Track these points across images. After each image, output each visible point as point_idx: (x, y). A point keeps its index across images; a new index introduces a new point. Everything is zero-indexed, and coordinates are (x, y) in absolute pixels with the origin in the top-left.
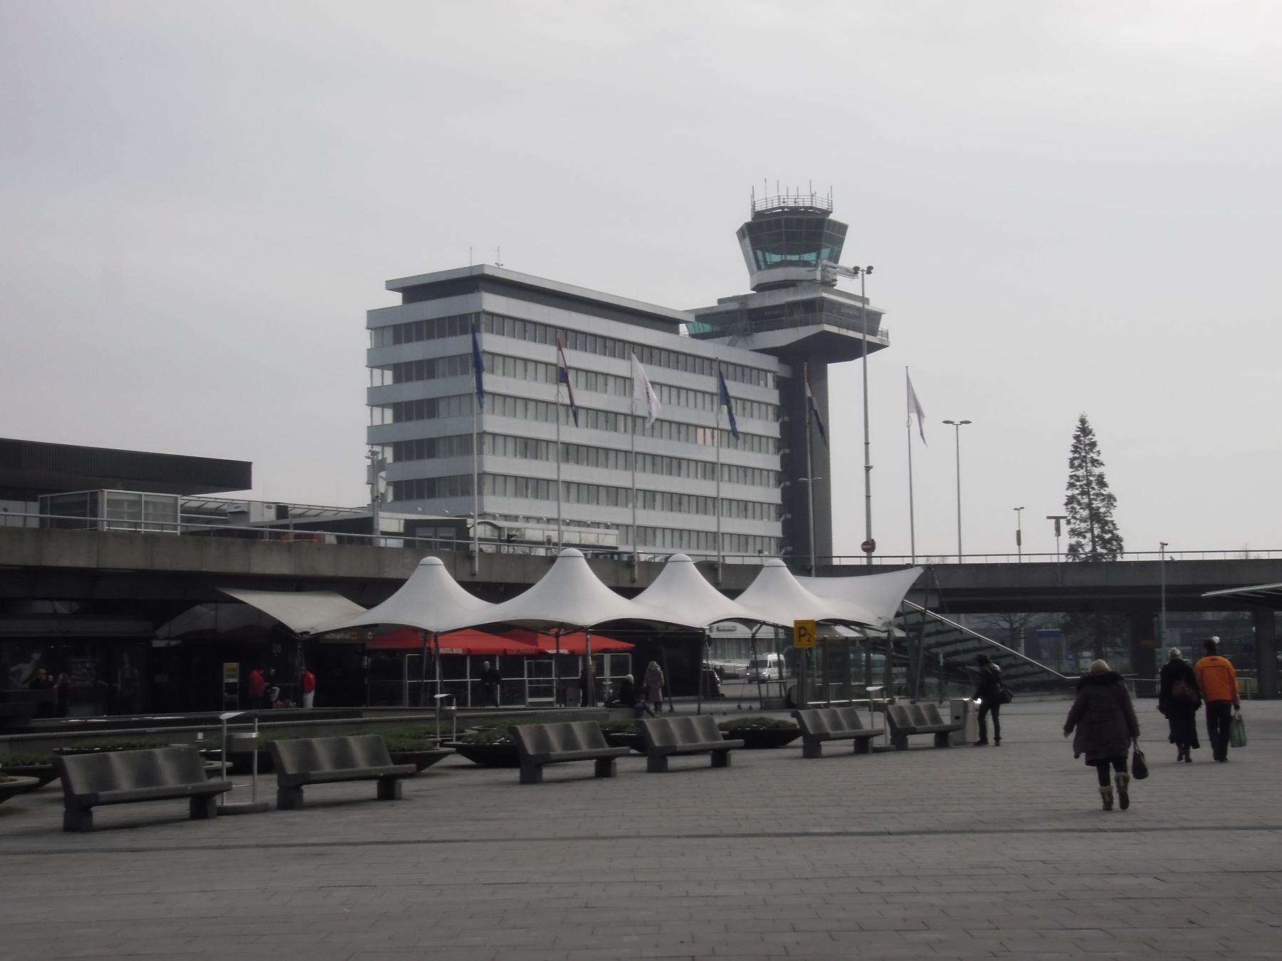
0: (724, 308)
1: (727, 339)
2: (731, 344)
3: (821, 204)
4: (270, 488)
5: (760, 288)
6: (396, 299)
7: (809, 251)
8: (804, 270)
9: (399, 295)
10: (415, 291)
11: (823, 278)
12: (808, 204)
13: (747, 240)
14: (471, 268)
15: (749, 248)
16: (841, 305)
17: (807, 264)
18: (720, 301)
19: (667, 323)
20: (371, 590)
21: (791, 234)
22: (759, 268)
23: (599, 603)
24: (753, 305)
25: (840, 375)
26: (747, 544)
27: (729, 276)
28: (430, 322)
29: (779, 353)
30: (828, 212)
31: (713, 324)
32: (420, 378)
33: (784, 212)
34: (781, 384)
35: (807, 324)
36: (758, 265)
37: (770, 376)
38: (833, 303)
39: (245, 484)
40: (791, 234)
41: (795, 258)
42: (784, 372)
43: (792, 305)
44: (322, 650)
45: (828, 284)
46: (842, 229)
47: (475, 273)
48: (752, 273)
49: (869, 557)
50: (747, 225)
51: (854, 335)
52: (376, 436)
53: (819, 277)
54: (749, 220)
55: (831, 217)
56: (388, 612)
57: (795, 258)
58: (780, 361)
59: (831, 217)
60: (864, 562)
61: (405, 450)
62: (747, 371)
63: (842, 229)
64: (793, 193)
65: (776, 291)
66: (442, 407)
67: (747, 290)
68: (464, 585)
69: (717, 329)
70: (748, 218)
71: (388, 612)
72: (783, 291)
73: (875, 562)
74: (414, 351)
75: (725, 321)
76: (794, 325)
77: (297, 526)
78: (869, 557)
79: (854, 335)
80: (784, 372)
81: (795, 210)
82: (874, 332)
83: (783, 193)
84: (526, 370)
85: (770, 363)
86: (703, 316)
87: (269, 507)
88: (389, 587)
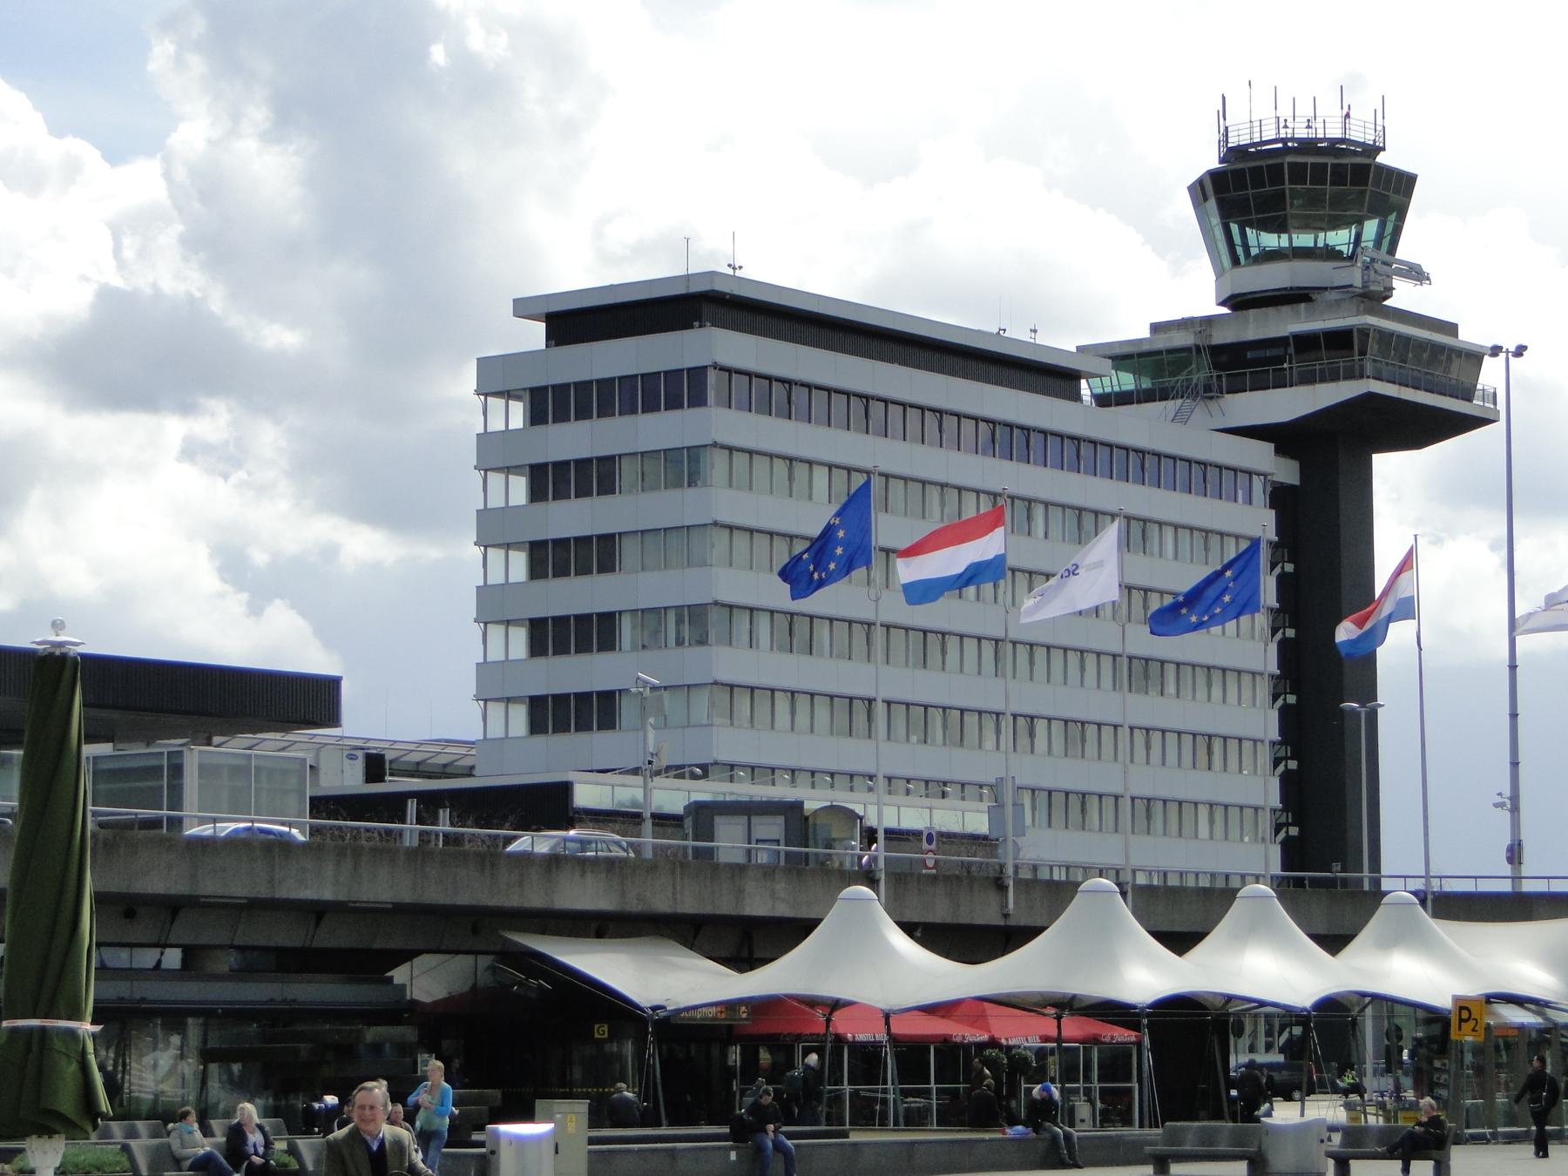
0: (1162, 343)
1: (1171, 405)
2: (1178, 418)
3: (1360, 133)
4: (365, 718)
5: (1238, 302)
6: (534, 335)
7: (1335, 224)
8: (1328, 266)
9: (540, 328)
10: (572, 322)
11: (1365, 284)
12: (1335, 132)
13: (1212, 204)
14: (688, 278)
15: (1215, 220)
16: (1406, 340)
17: (1331, 254)
18: (1156, 328)
19: (1054, 377)
20: (747, 942)
21: (1297, 194)
22: (1236, 261)
23: (1146, 975)
24: (1221, 337)
25: (1396, 476)
26: (1149, 816)
27: (1170, 280)
28: (605, 384)
29: (1281, 437)
30: (1377, 149)
31: (1137, 372)
32: (583, 492)
33: (1286, 150)
34: (1280, 497)
35: (1335, 378)
36: (1234, 255)
37: (1257, 483)
38: (1385, 337)
39: (331, 717)
40: (1297, 194)
41: (1304, 240)
42: (1287, 472)
43: (1306, 343)
44: (685, 1040)
45: (1374, 298)
46: (1404, 183)
47: (695, 288)
48: (1220, 273)
49: (1516, 878)
50: (1214, 175)
51: (1427, 391)
52: (492, 606)
53: (1358, 283)
54: (1214, 164)
55: (1382, 159)
56: (778, 977)
57: (1304, 240)
58: (1279, 451)
59: (1382, 159)
60: (1505, 886)
61: (548, 636)
62: (1212, 473)
63: (1404, 183)
64: (1305, 111)
65: (1271, 311)
66: (629, 552)
67: (1213, 309)
68: (909, 928)
69: (1146, 384)
70: (1210, 160)
71: (778, 977)
72: (1285, 309)
73: (1528, 887)
74: (573, 440)
75: (1172, 366)
76: (1308, 379)
77: (430, 803)
78: (1516, 878)
79: (1427, 391)
80: (1287, 472)
81: (1308, 146)
82: (1467, 394)
83: (1285, 112)
84: (791, 478)
85: (1260, 455)
86: (1124, 357)
87: (352, 757)
88: (791, 932)
